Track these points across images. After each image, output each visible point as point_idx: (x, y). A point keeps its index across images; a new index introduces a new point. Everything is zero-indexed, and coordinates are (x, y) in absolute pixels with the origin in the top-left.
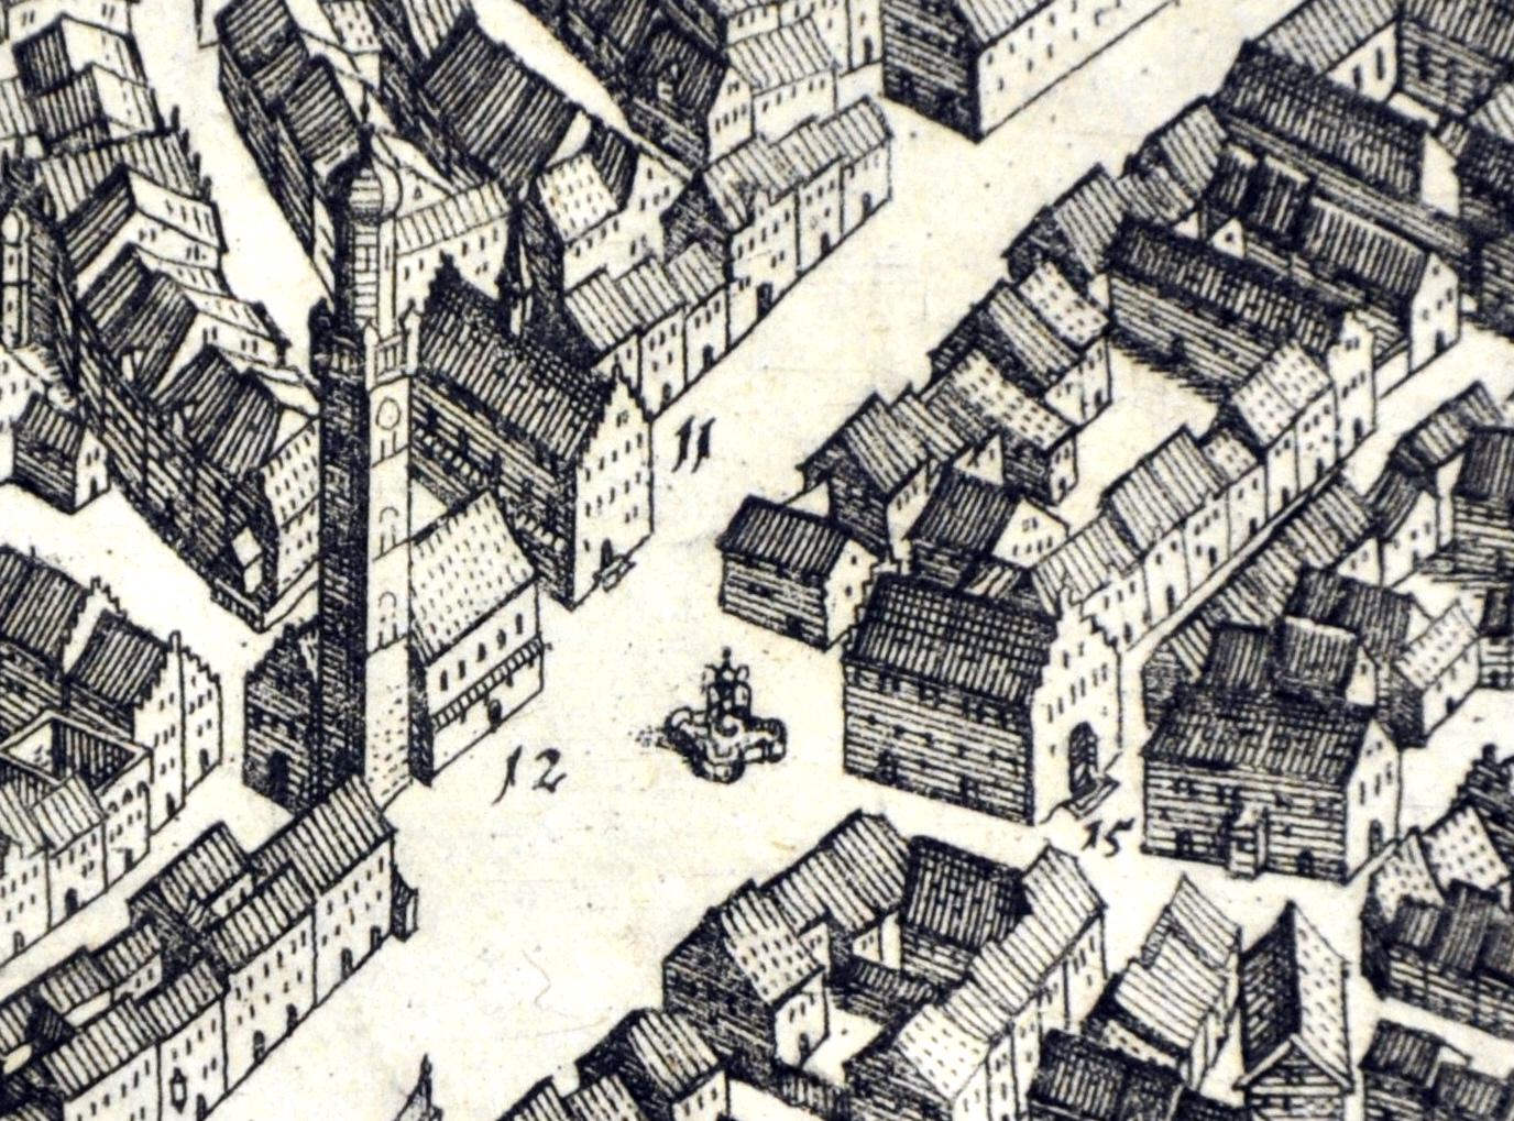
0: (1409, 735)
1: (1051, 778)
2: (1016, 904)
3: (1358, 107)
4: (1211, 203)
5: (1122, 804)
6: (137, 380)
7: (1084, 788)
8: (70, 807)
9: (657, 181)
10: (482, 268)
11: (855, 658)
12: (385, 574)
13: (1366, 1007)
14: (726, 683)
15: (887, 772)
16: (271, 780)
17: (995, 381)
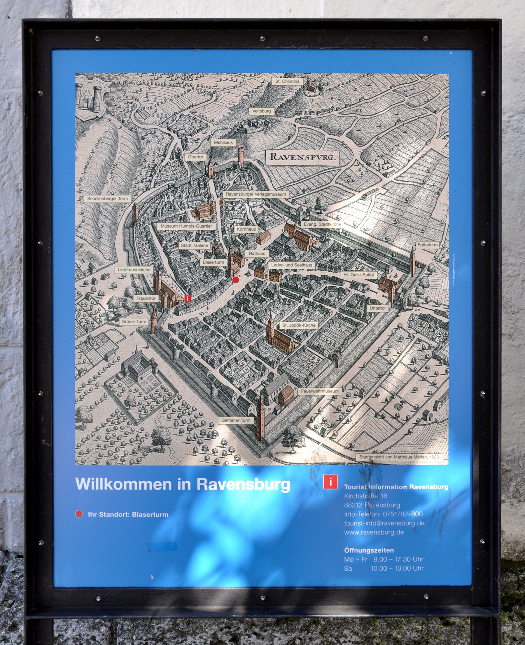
0: (282, 275)
1: (264, 277)
2: (263, 283)
3: (279, 243)
4: (272, 248)
5: (268, 278)
6: (388, 541)
7: (266, 277)
8: (216, 278)
9: (245, 247)
10: (236, 251)
11: (255, 271)
12: (232, 266)
13: (280, 288)
14: (248, 272)
15: (256, 276)
16: (226, 277)
17: (102, 163)
